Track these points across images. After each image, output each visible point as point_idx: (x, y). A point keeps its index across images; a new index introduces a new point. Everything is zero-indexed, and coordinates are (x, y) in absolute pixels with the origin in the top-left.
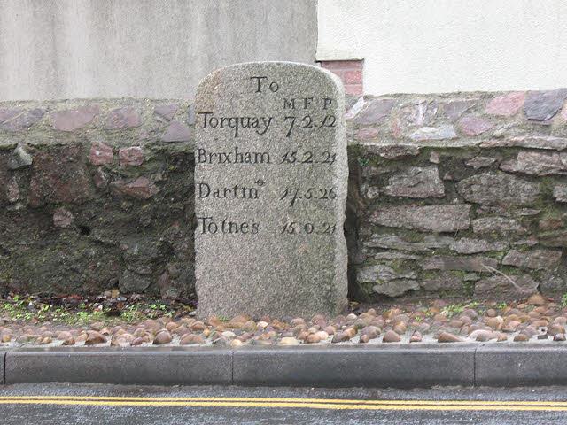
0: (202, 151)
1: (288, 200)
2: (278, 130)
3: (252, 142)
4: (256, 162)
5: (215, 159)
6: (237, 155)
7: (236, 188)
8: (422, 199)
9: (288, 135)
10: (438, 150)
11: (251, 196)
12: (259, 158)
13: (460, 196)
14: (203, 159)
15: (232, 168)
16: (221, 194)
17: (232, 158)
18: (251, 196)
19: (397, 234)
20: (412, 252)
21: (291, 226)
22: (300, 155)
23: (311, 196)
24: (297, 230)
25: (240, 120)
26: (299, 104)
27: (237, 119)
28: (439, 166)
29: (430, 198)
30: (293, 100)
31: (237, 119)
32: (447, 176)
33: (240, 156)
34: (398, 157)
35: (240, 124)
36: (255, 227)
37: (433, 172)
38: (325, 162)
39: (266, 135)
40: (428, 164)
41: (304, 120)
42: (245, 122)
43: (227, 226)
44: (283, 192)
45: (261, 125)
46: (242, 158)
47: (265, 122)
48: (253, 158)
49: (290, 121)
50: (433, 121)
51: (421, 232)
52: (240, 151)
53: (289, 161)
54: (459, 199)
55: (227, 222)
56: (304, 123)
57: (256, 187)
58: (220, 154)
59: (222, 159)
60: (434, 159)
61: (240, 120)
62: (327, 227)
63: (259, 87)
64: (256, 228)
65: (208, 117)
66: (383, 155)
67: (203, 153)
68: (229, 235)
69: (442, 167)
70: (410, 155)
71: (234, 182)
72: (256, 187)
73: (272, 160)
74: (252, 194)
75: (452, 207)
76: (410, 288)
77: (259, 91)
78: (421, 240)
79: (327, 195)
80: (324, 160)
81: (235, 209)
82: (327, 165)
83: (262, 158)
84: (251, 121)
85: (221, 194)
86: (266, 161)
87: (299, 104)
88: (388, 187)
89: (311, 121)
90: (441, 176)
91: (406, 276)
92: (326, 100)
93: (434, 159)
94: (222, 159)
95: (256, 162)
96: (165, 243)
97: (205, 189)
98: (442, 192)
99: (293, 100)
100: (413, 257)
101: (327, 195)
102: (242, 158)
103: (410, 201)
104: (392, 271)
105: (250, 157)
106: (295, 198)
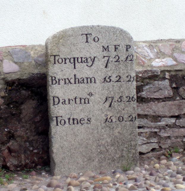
0: (54, 78)
1: (107, 104)
2: (100, 64)
3: (84, 71)
4: (87, 82)
5: (62, 82)
6: (75, 79)
7: (75, 98)
8: (161, 99)
9: (106, 67)
10: (169, 71)
11: (85, 103)
12: (89, 80)
13: (180, 96)
14: (54, 82)
15: (74, 86)
16: (67, 102)
17: (72, 81)
18: (85, 103)
19: (147, 119)
20: (155, 128)
21: (110, 118)
22: (114, 78)
23: (121, 100)
24: (114, 120)
25: (76, 59)
26: (112, 48)
27: (74, 58)
28: (170, 80)
29: (165, 98)
30: (108, 47)
31: (74, 58)
32: (174, 85)
33: (77, 80)
34: (149, 76)
35: (76, 62)
36: (89, 120)
37: (166, 83)
38: (129, 81)
39: (93, 67)
40: (164, 78)
41: (115, 58)
42: (80, 60)
43: (71, 121)
44: (104, 99)
45: (91, 61)
46: (78, 81)
47: (91, 59)
48: (85, 81)
49: (106, 58)
50: (160, 54)
51: (156, 118)
52: (77, 76)
53: (107, 81)
54: (180, 98)
55: (72, 118)
56: (115, 60)
57: (88, 97)
58: (65, 79)
59: (67, 81)
60: (167, 75)
61: (76, 59)
62: (131, 117)
63: (87, 40)
64: (89, 121)
65: (57, 58)
66: (140, 75)
67: (54, 79)
68: (73, 125)
69: (171, 80)
70: (156, 75)
71: (75, 95)
72: (88, 97)
73: (97, 81)
74: (86, 101)
75: (176, 102)
76: (154, 147)
77: (87, 42)
78: (160, 121)
79: (131, 100)
80: (128, 80)
81: (79, 111)
82: (130, 83)
83: (90, 80)
84: (83, 59)
85: (67, 102)
86: (94, 82)
87: (112, 48)
88: (143, 93)
89: (119, 58)
90: (171, 86)
91: (152, 141)
92: (127, 46)
93: (167, 75)
94: (67, 81)
95: (87, 82)
96: (9, 132)
97: (56, 100)
98: (172, 94)
99: (108, 47)
100: (156, 130)
101: (131, 100)
102: (78, 81)
103: (155, 100)
104: (144, 139)
105: (83, 80)
106: (112, 102)
